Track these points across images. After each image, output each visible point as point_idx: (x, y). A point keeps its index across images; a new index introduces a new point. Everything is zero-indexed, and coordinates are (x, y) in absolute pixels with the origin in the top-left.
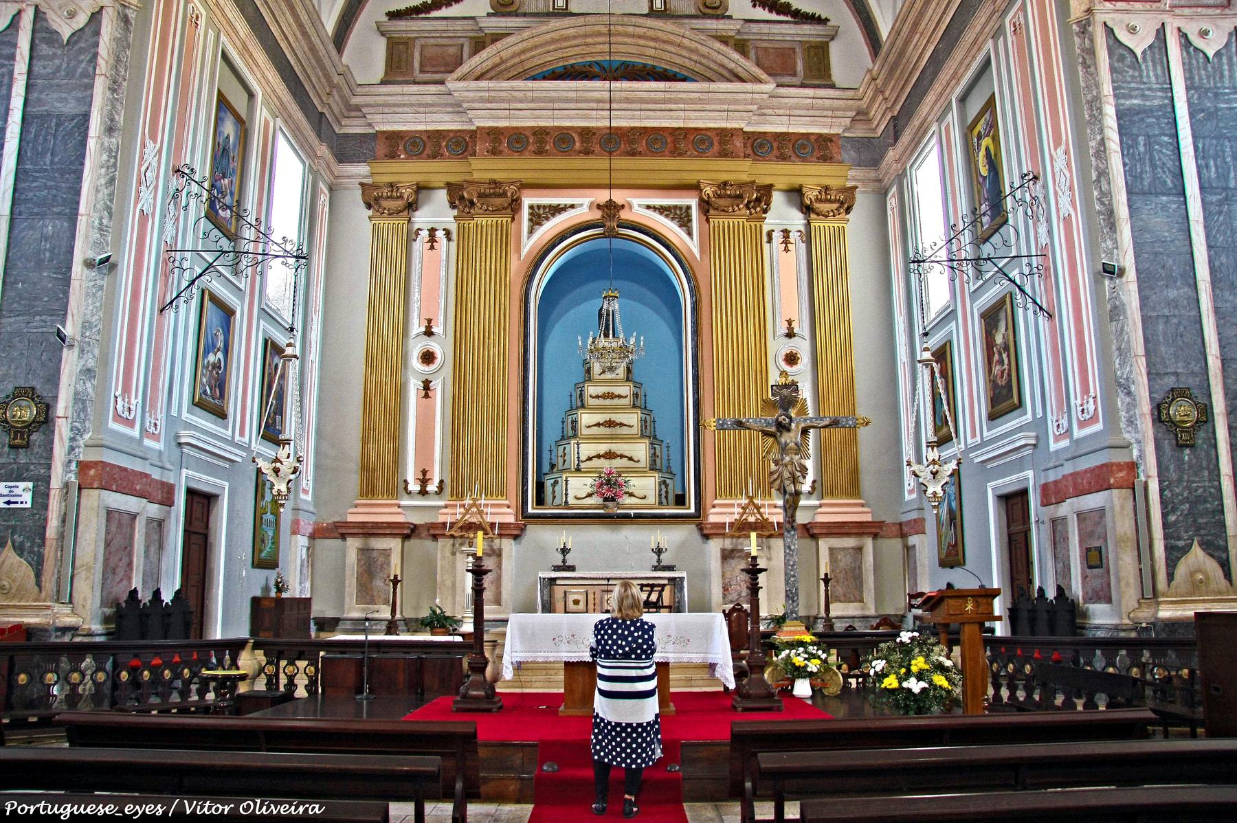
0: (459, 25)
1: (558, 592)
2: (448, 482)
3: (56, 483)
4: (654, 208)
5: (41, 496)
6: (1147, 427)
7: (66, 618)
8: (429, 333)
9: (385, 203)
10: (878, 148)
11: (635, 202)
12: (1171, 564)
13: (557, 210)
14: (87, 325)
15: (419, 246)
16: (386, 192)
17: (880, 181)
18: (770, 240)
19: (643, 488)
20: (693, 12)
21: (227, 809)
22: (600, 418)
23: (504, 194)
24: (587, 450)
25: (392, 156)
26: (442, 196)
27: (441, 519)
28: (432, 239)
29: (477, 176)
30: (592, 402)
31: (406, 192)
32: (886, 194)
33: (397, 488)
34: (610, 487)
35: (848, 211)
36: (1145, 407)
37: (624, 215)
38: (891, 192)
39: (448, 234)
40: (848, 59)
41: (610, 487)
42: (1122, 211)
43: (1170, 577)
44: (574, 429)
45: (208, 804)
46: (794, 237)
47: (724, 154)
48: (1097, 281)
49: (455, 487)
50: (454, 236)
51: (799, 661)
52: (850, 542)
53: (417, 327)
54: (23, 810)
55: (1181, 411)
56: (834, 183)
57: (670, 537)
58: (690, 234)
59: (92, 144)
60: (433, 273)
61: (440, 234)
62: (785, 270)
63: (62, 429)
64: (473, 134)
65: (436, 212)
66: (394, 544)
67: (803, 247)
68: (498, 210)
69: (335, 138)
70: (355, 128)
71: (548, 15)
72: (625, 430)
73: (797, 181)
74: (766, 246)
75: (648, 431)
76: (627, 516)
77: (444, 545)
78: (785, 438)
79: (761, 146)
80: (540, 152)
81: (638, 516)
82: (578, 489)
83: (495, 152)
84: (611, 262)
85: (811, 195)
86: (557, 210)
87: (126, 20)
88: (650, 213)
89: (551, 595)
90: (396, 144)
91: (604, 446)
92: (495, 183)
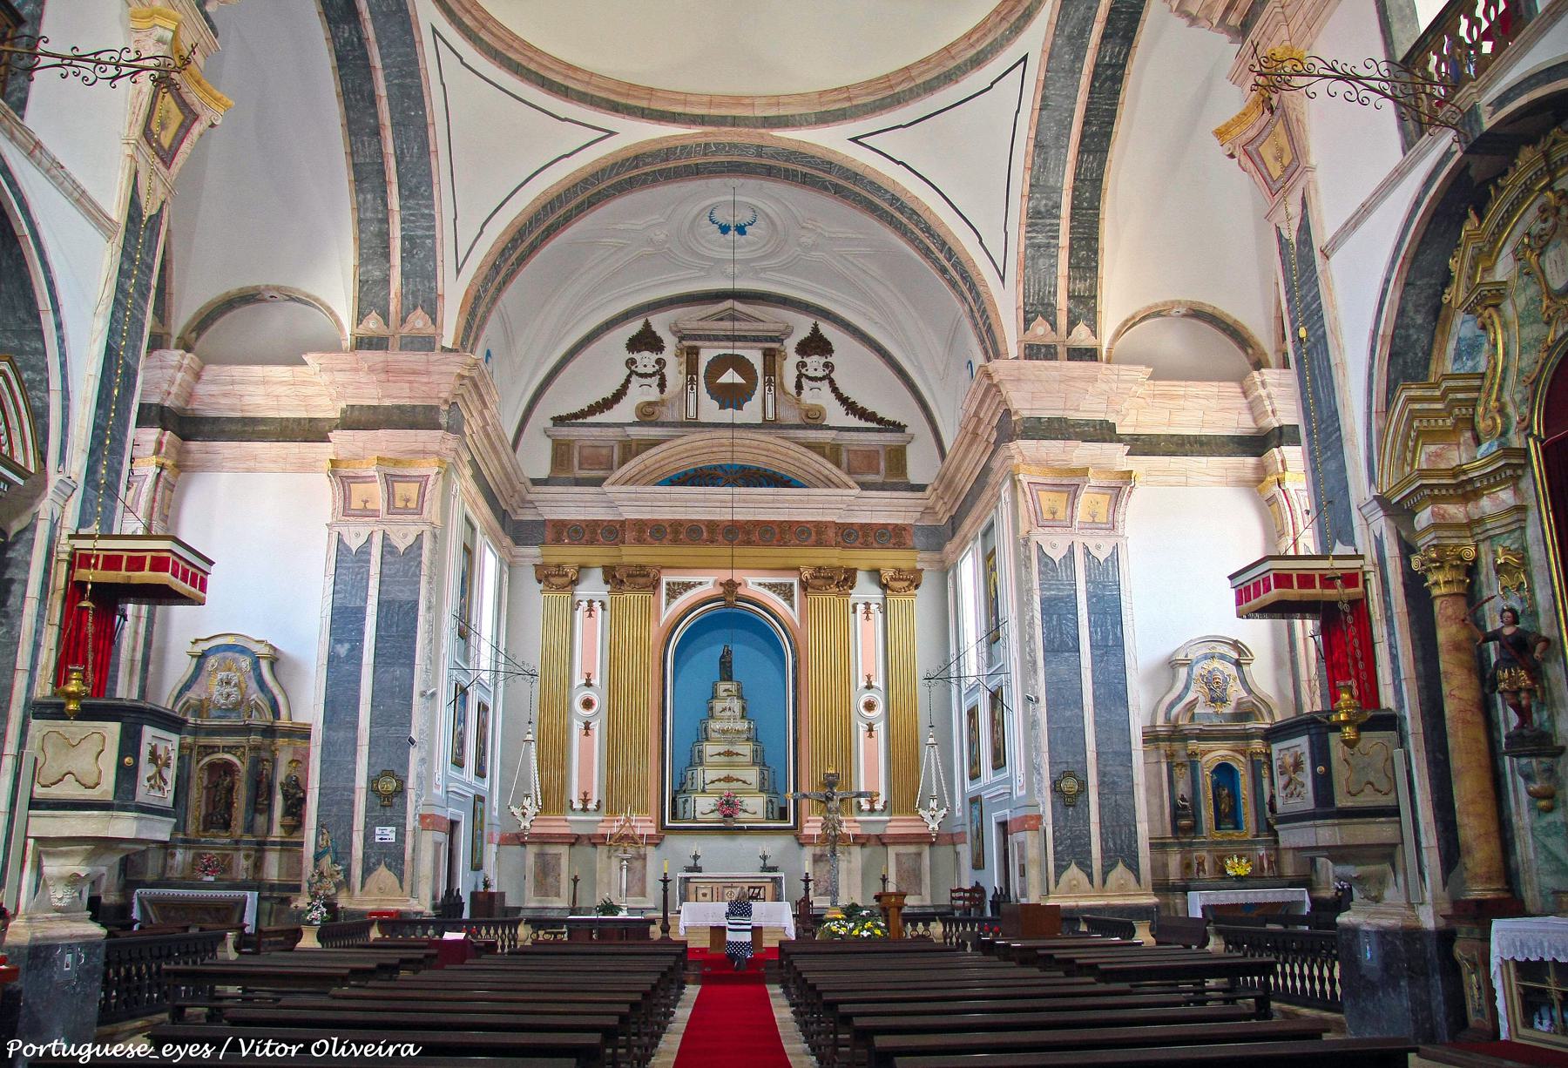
0: (611, 432)
1: (692, 887)
2: (604, 802)
3: (409, 828)
4: (765, 585)
5: (401, 835)
6: (1047, 794)
7: (419, 908)
8: (588, 684)
9: (552, 580)
10: (941, 536)
11: (750, 580)
12: (1058, 875)
13: (688, 586)
14: (421, 732)
15: (579, 614)
16: (554, 571)
17: (943, 562)
18: (855, 611)
19: (754, 806)
20: (797, 421)
21: (294, 1049)
22: (722, 749)
23: (648, 575)
24: (711, 774)
25: (558, 540)
26: (598, 574)
27: (600, 831)
28: (590, 609)
29: (625, 560)
30: (714, 735)
31: (571, 572)
32: (947, 573)
33: (564, 806)
34: (728, 806)
35: (917, 587)
36: (1047, 783)
37: (741, 591)
38: (946, 572)
39: (603, 605)
40: (921, 465)
41: (728, 806)
42: (1040, 662)
43: (1057, 883)
44: (700, 758)
45: (269, 1043)
46: (873, 607)
47: (820, 543)
48: (1025, 706)
49: (611, 805)
50: (608, 606)
51: (834, 928)
52: (912, 849)
53: (579, 680)
54: (29, 1050)
55: (1069, 785)
56: (903, 565)
57: (774, 846)
58: (792, 606)
59: (421, 619)
60: (590, 638)
61: (597, 605)
62: (866, 636)
63: (411, 795)
64: (623, 523)
65: (593, 587)
66: (563, 850)
67: (880, 616)
68: (643, 587)
69: (517, 530)
70: (527, 515)
71: (682, 425)
72: (740, 759)
73: (877, 564)
74: (851, 616)
75: (759, 760)
76: (741, 829)
77: (602, 851)
78: (830, 805)
79: (849, 535)
80: (675, 541)
81: (749, 829)
82: (704, 806)
83: (640, 541)
84: (730, 620)
85: (887, 575)
86: (688, 586)
87: (435, 536)
88: (761, 589)
89: (686, 889)
90: (563, 532)
91: (725, 773)
92: (642, 567)
